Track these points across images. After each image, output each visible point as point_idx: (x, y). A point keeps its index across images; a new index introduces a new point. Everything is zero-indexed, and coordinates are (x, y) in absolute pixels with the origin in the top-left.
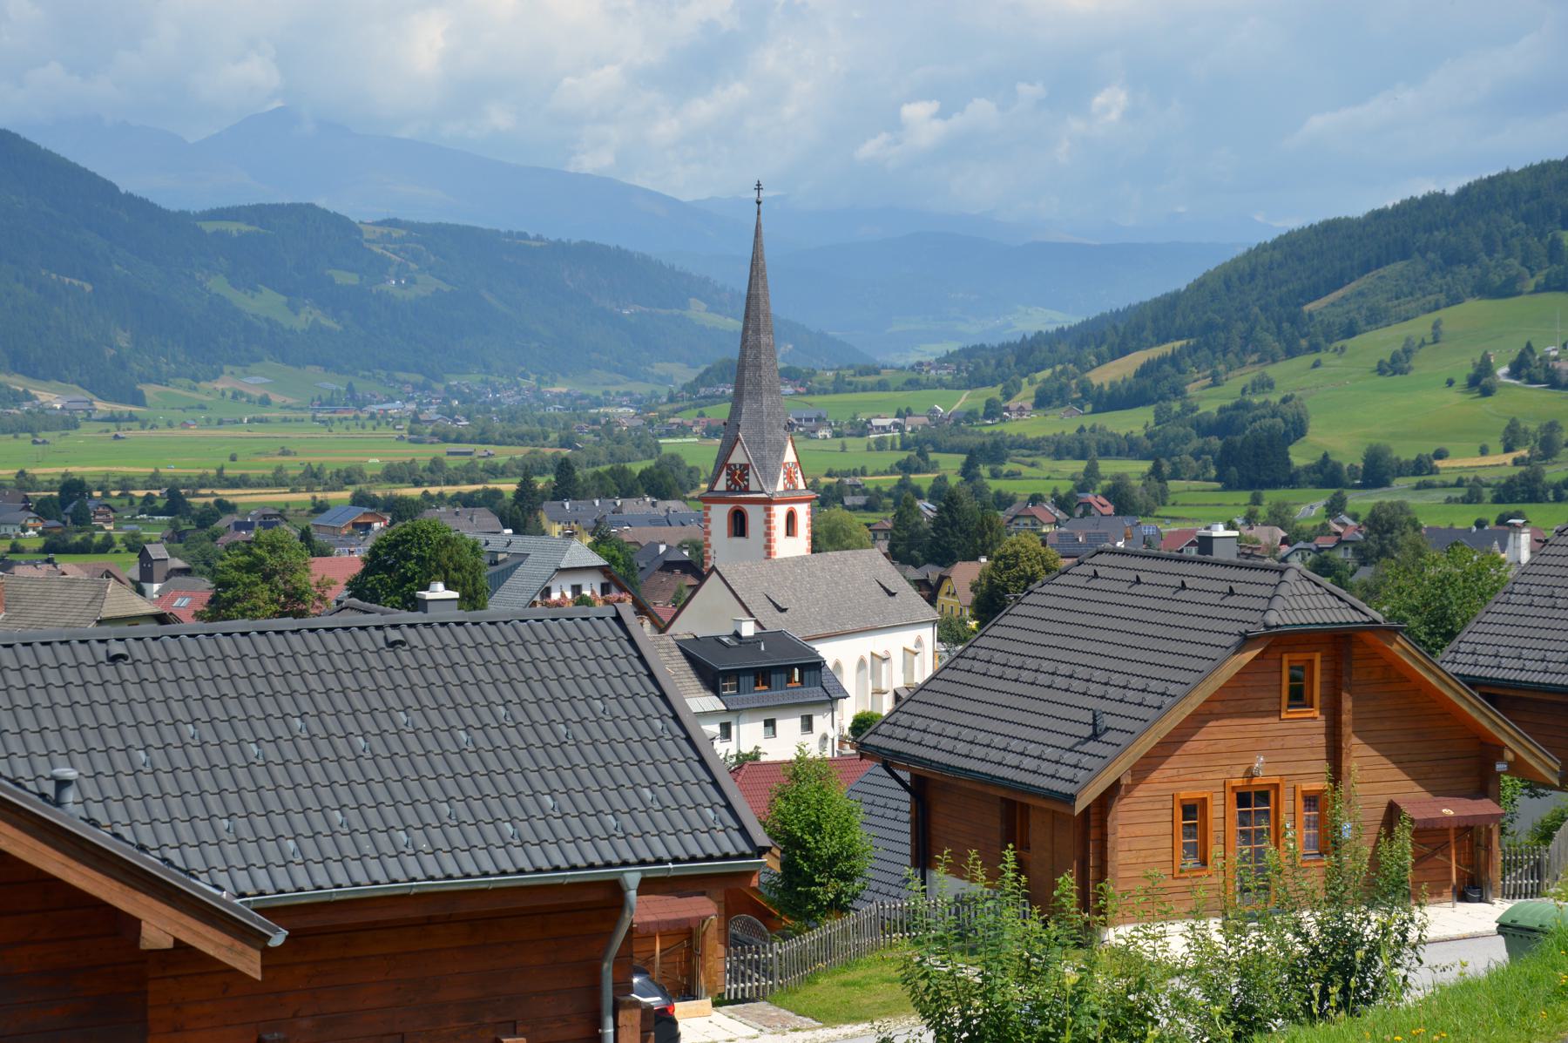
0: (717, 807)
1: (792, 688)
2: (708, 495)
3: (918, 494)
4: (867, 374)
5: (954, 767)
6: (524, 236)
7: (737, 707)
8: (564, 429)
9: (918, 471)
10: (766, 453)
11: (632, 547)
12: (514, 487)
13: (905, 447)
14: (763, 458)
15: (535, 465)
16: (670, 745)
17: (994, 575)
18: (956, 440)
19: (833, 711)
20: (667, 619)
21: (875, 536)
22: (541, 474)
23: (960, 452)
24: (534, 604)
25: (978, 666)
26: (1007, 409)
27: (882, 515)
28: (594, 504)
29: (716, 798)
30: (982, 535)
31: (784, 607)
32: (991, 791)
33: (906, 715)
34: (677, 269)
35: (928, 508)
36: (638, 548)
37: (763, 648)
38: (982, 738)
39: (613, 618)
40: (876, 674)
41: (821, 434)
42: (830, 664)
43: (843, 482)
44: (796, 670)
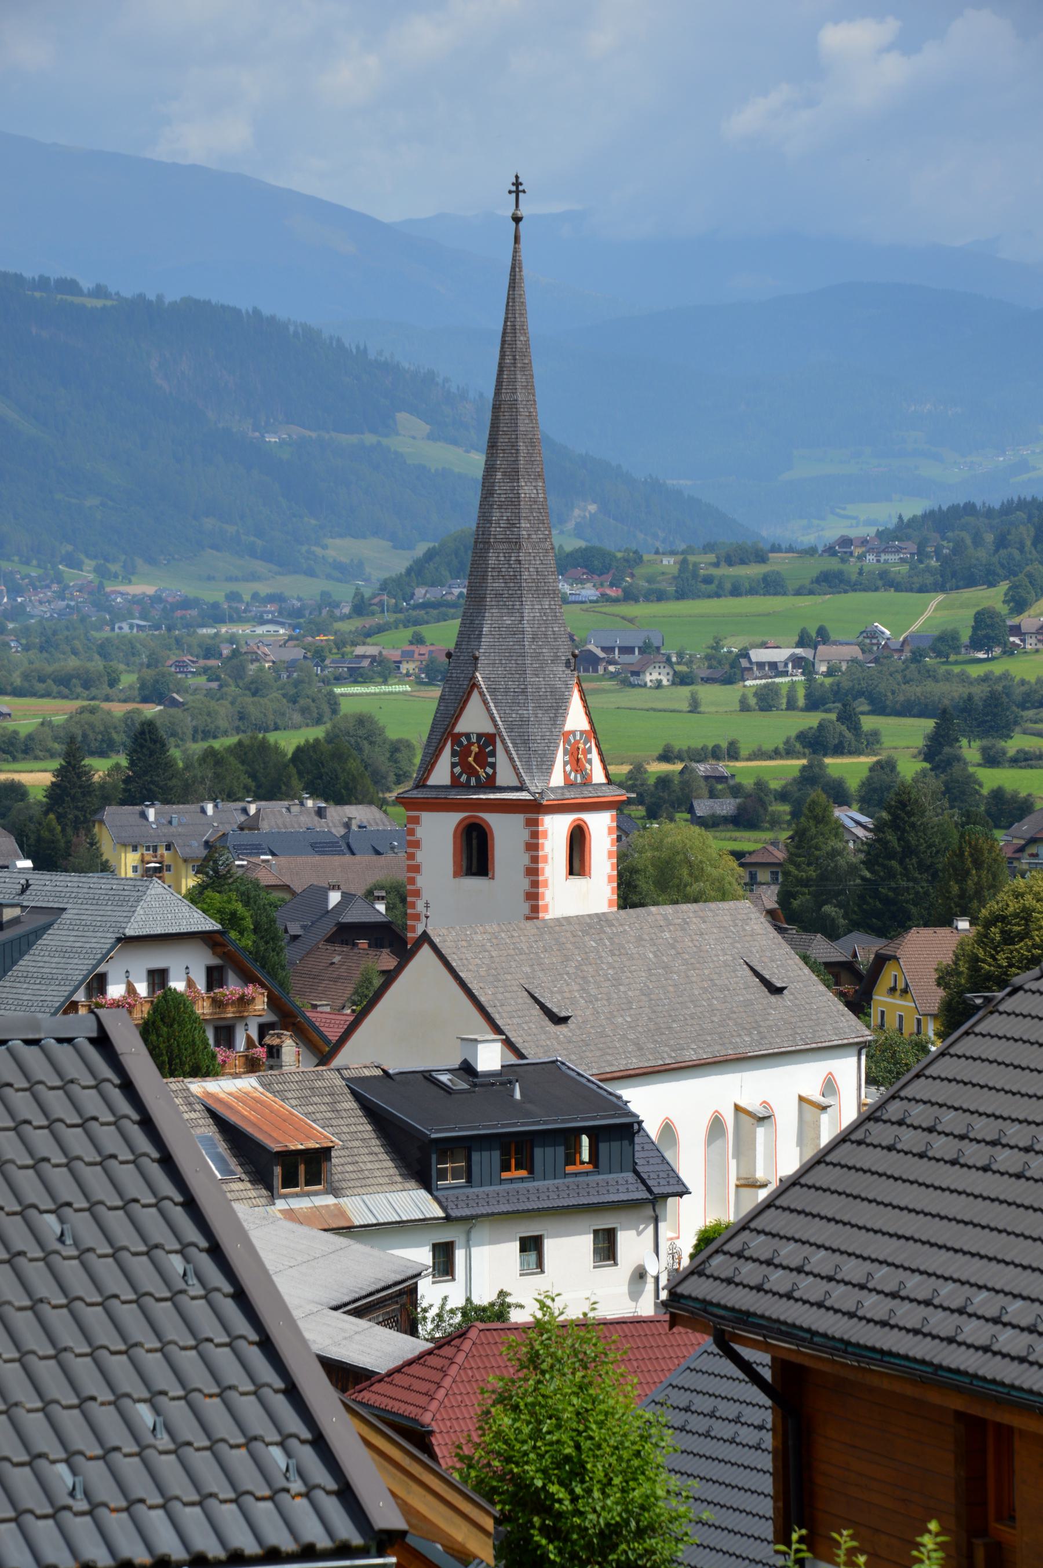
0: (293, 1443)
1: (576, 1174)
2: (415, 794)
3: (839, 795)
4: (743, 562)
5: (858, 1345)
6: (69, 286)
7: (467, 1212)
8: (149, 666)
9: (839, 750)
10: (528, 712)
11: (276, 896)
12: (46, 778)
13: (814, 704)
14: (524, 722)
15: (91, 736)
16: (199, 1310)
17: (981, 953)
18: (915, 691)
19: (656, 1221)
20: (333, 1036)
21: (753, 876)
22: (102, 754)
23: (922, 714)
24: (73, 1006)
25: (909, 1139)
26: (1016, 630)
27: (768, 836)
28: (203, 811)
29: (294, 1424)
30: (962, 875)
31: (563, 1014)
32: (934, 1397)
33: (762, 1237)
34: (372, 355)
35: (858, 823)
36: (287, 896)
37: (518, 1095)
38: (915, 1286)
39: (92, 1041)
40: (744, 1148)
41: (651, 677)
42: (652, 1128)
43: (693, 770)
44: (585, 1140)
